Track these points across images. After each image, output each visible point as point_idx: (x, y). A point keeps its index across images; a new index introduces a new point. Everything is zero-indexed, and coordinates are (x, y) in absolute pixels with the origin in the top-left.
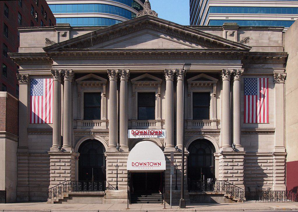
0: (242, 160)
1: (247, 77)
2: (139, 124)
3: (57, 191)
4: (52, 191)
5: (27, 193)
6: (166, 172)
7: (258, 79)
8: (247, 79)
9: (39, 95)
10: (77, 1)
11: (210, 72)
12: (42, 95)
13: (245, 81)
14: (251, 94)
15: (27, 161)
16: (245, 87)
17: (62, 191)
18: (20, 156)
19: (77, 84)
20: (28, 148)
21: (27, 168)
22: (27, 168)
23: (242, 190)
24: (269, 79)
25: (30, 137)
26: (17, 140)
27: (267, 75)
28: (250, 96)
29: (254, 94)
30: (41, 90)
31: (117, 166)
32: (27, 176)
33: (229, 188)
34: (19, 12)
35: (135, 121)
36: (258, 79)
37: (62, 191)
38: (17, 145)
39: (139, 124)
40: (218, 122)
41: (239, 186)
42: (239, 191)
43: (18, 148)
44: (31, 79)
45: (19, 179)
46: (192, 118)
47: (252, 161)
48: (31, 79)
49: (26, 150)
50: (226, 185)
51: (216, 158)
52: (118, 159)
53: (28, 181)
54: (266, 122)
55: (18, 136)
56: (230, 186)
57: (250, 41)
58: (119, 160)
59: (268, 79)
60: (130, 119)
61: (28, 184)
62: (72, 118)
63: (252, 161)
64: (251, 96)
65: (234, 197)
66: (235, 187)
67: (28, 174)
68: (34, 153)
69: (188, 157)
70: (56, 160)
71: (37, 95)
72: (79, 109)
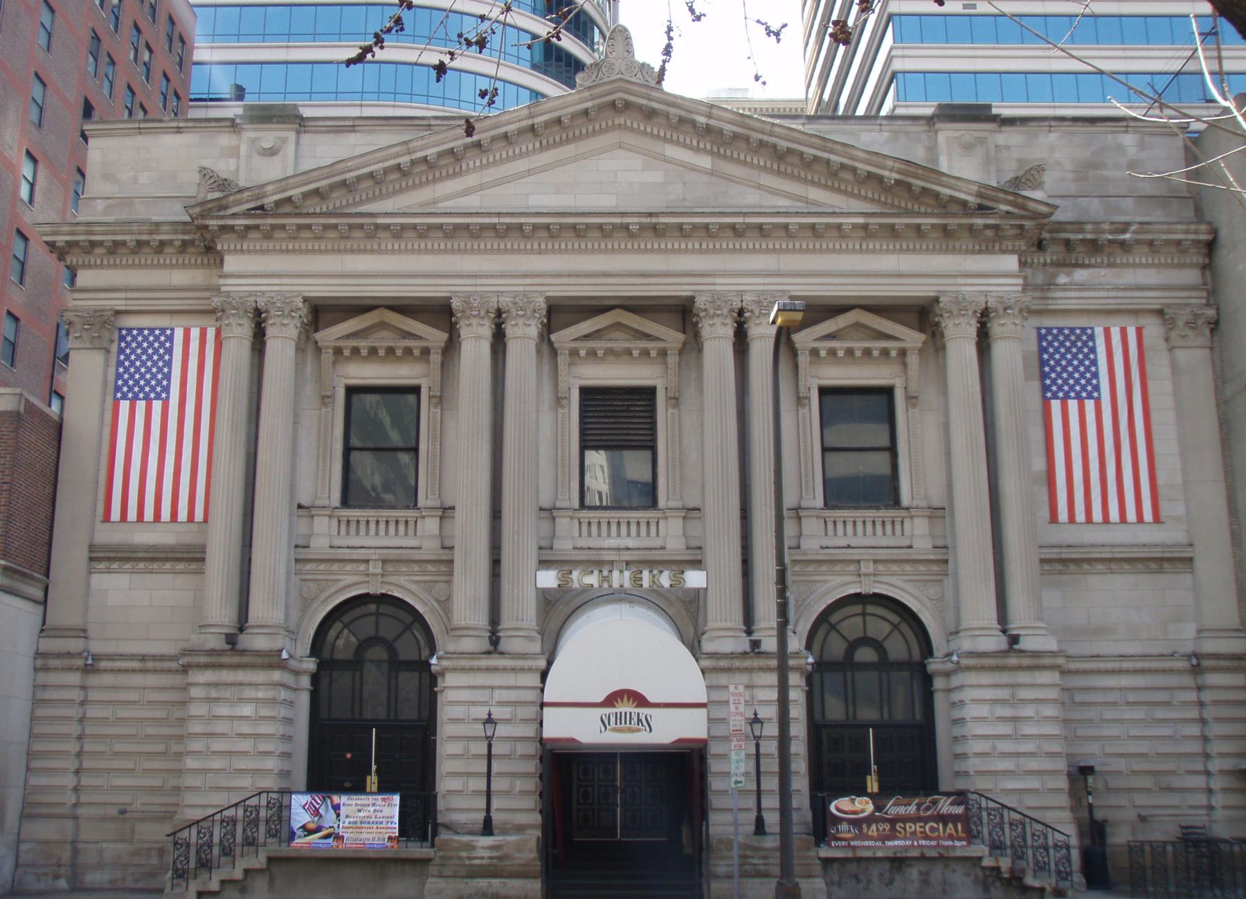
0: (1053, 694)
1: (1049, 322)
2: (585, 528)
3: (216, 840)
4: (194, 840)
5: (69, 847)
6: (714, 749)
7: (1099, 332)
8: (1049, 330)
9: (152, 395)
10: (1115, 4)
11: (406, 302)
12: (164, 395)
13: (1041, 338)
14: (1072, 394)
15: (76, 695)
16: (1043, 363)
17: (239, 838)
18: (46, 669)
19: (318, 350)
20: (85, 631)
21: (74, 729)
22: (74, 729)
23: (1063, 838)
24: (1145, 332)
25: (100, 581)
26: (38, 593)
27: (1136, 312)
28: (1070, 401)
29: (1084, 394)
30: (163, 374)
31: (490, 720)
32: (72, 764)
33: (1002, 829)
34: (37, 75)
35: (570, 513)
36: (1099, 332)
37: (239, 838)
38: (39, 619)
39: (585, 528)
40: (939, 513)
41: (1049, 817)
42: (1050, 843)
43: (42, 631)
44: (120, 329)
45: (34, 781)
46: (819, 502)
47: (1098, 697)
48: (120, 329)
49: (74, 645)
50: (984, 814)
51: (938, 683)
52: (492, 688)
53: (76, 789)
54: (1148, 515)
55: (47, 575)
56: (1006, 819)
57: (1049, 178)
58: (497, 692)
59: (1139, 331)
60: (304, 503)
61: (75, 805)
62: (291, 502)
63: (1098, 697)
64: (141, 405)
65: (1029, 874)
66: (1028, 820)
67: (79, 754)
68: (110, 657)
69: (809, 679)
70: (468, 692)
71: (141, 395)
72: (324, 459)
